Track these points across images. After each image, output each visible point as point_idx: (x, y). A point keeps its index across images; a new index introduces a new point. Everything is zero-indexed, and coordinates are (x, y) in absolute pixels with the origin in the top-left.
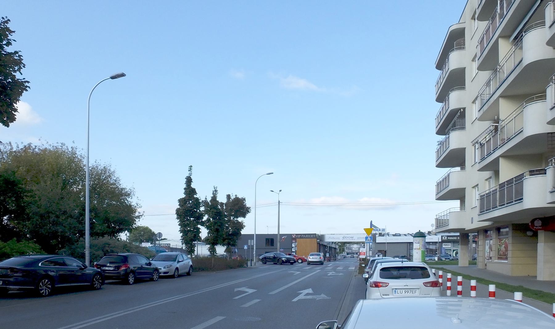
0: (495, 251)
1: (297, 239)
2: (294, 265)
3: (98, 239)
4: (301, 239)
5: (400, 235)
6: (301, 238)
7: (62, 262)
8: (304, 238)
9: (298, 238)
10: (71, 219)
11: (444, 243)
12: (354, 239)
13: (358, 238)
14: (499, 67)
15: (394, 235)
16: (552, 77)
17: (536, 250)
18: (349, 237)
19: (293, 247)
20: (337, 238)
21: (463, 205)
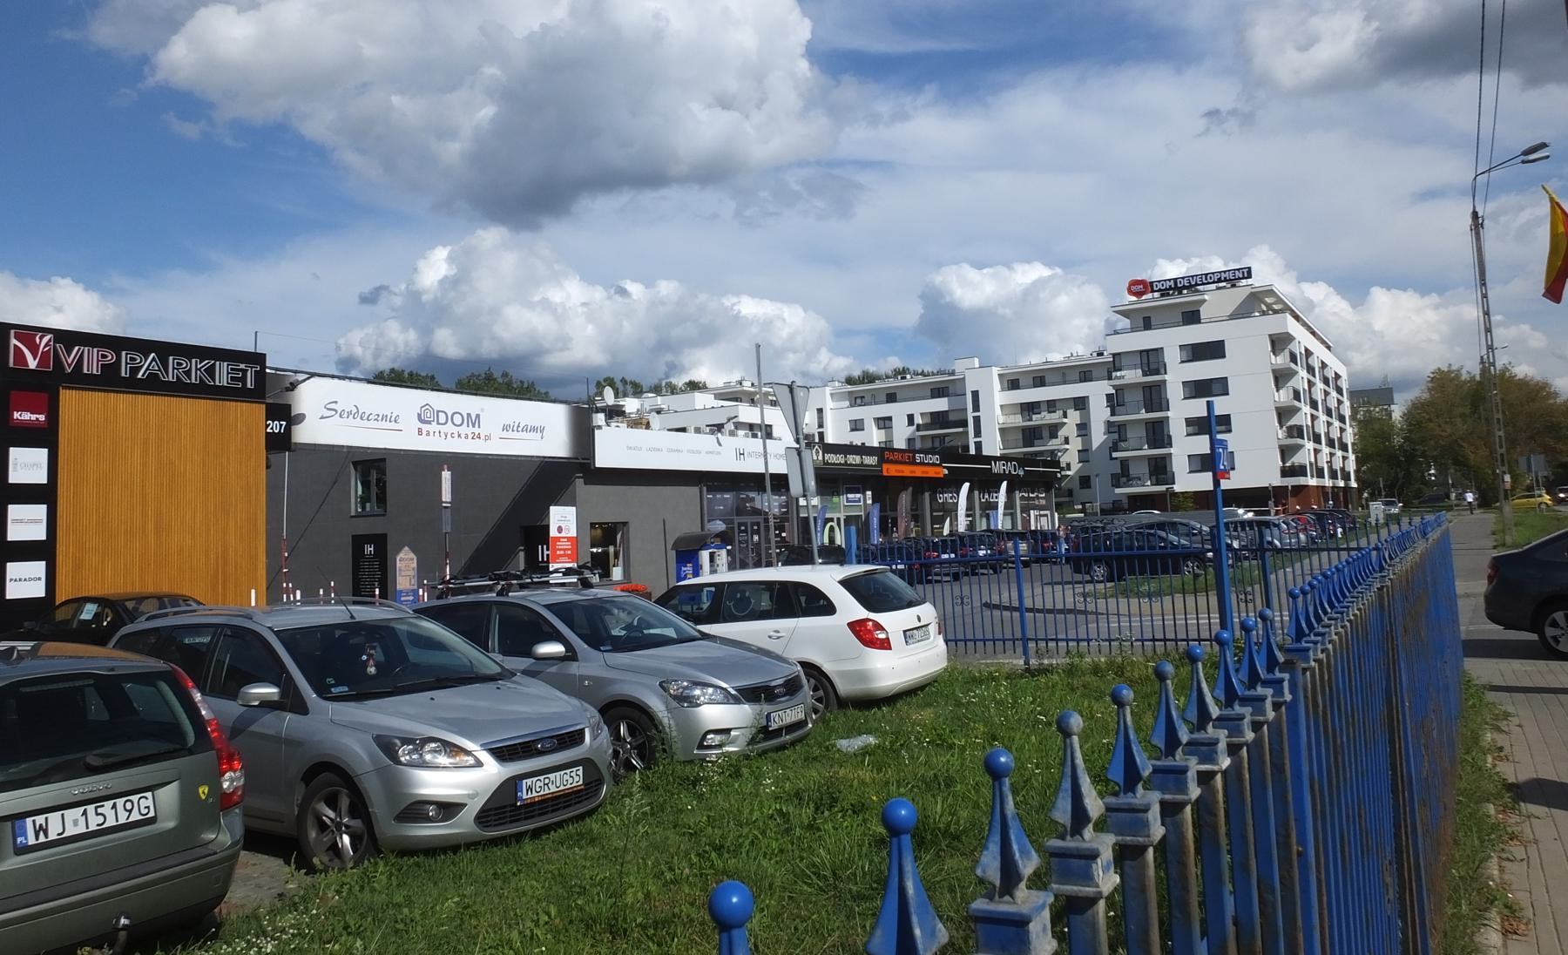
0: (1388, 526)
1: (69, 399)
2: (778, 571)
3: (378, 415)
4: (122, 402)
5: (640, 449)
6: (109, 380)
7: (1109, 409)
8: (153, 385)
9: (79, 380)
10: (1349, 438)
11: (1319, 666)
12: (483, 431)
13: (505, 428)
14: (832, 540)
15: (707, 453)
16: (556, 637)
17: (595, 708)
18: (457, 419)
19: (749, 598)
20: (384, 418)
21: (608, 606)
